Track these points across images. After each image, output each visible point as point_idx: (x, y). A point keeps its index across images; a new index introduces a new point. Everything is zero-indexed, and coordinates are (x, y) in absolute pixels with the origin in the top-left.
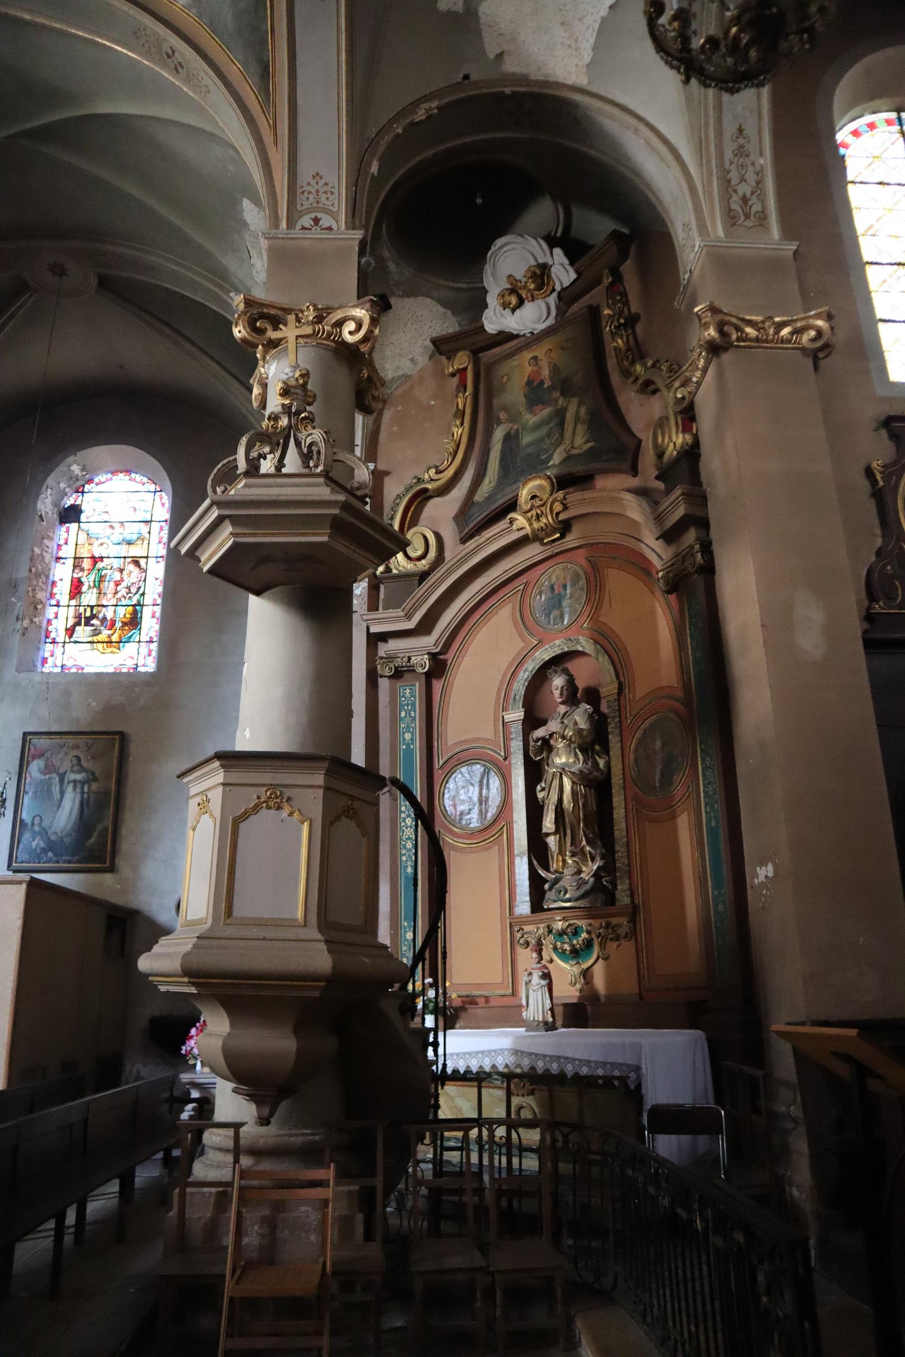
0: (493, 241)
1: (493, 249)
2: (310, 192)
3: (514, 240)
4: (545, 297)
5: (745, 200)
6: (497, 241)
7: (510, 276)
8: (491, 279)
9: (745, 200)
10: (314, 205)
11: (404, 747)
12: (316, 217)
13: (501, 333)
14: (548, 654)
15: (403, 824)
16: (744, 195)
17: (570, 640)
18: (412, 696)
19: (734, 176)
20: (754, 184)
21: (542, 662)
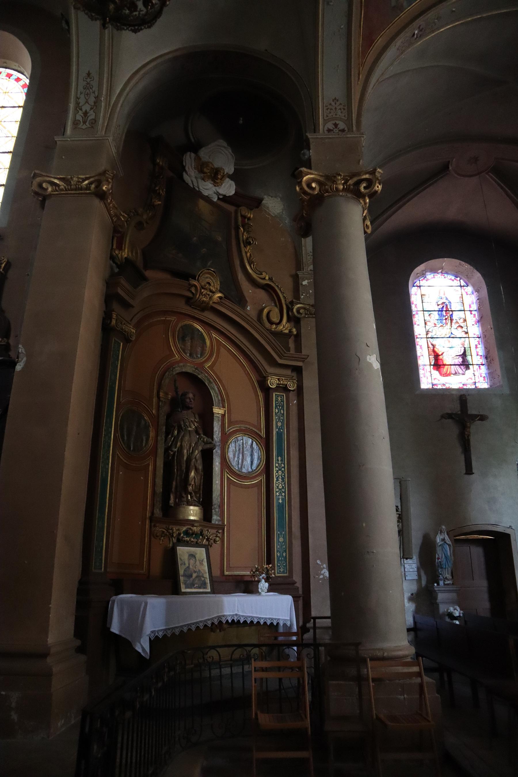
2: (331, 109)
5: (86, 113)
9: (86, 113)
10: (334, 116)
11: (283, 533)
12: (336, 123)
15: (283, 485)
16: (86, 111)
18: (279, 566)
19: (82, 101)
20: (93, 104)
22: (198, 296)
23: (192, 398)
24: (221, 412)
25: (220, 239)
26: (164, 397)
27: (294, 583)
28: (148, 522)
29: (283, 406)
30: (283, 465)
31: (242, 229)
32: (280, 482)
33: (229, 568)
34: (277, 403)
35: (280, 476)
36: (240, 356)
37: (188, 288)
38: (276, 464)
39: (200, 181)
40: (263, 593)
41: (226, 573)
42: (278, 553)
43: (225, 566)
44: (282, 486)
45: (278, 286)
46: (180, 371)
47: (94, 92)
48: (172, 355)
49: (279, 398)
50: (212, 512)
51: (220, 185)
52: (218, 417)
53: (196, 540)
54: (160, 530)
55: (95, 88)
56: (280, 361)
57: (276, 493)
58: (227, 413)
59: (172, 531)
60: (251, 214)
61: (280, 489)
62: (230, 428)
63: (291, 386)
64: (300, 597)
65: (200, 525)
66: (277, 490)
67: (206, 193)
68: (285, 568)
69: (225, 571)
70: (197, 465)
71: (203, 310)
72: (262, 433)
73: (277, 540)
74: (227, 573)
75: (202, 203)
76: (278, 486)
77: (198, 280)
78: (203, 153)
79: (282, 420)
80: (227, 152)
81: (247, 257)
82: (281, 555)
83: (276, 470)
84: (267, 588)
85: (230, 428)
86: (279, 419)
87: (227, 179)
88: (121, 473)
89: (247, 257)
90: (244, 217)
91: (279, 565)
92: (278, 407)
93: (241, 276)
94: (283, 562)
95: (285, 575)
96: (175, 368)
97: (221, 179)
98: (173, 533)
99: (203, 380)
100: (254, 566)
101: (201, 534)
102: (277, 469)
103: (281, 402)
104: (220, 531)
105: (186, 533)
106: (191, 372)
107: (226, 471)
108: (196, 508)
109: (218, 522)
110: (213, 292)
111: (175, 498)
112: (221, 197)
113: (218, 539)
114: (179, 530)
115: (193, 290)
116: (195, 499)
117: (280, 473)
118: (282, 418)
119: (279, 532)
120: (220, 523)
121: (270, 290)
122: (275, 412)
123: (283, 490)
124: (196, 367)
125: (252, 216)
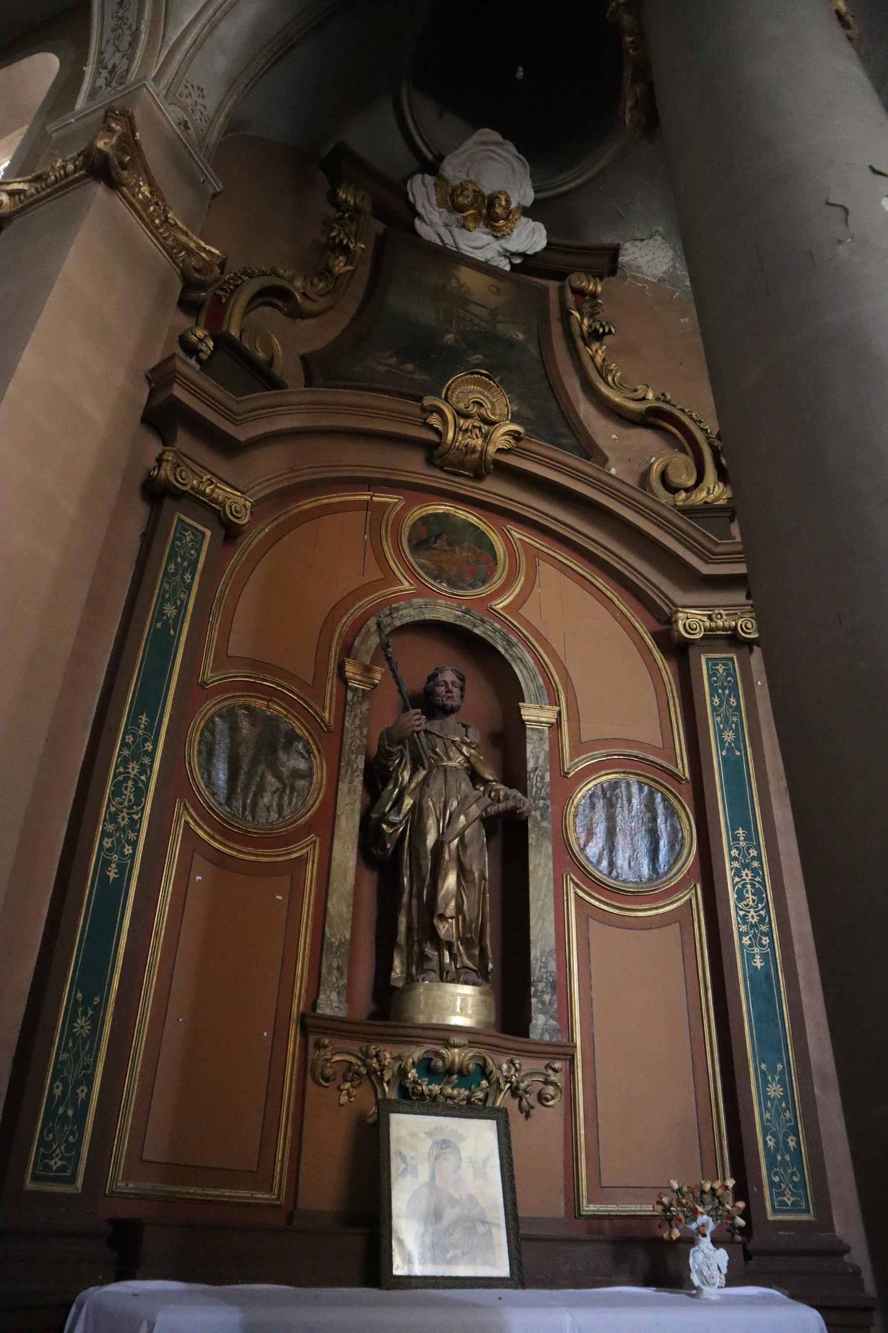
11: (779, 1066)
15: (762, 913)
22: (450, 435)
23: (453, 683)
24: (548, 715)
25: (521, 337)
26: (358, 677)
27: (840, 1250)
28: (293, 1030)
29: (734, 688)
30: (753, 853)
31: (577, 315)
32: (751, 903)
33: (598, 1191)
34: (716, 682)
35: (749, 886)
36: (595, 579)
37: (422, 421)
38: (730, 850)
39: (457, 231)
40: (711, 1292)
41: (589, 1208)
42: (768, 1138)
43: (584, 1184)
44: (760, 915)
45: (682, 410)
46: (417, 619)
47: (130, 27)
48: (390, 579)
49: (721, 668)
50: (530, 1004)
51: (509, 234)
52: (541, 732)
53: (467, 1093)
54: (337, 1058)
55: (132, 20)
56: (706, 569)
57: (741, 940)
58: (568, 720)
59: (379, 1061)
60: (595, 285)
61: (752, 926)
62: (577, 760)
63: (748, 629)
64: (868, 1310)
65: (469, 1042)
66: (744, 928)
67: (480, 255)
68: (801, 1191)
69: (584, 1202)
70: (466, 861)
71: (478, 477)
72: (680, 766)
73: (759, 1094)
74: (592, 1207)
75: (466, 274)
76: (745, 915)
77: (446, 399)
78: (452, 169)
79: (182, 602)
80: (504, 154)
81: (596, 366)
82: (781, 1146)
83: (732, 869)
84: (725, 1271)
85: (577, 760)
86: (726, 721)
87: (524, 220)
88: (199, 878)
89: (596, 366)
90: (579, 293)
91: (776, 1179)
92: (720, 691)
93: (585, 410)
94: (789, 1171)
95: (805, 1217)
96: (397, 609)
97: (506, 219)
98: (383, 1068)
99: (490, 640)
100: (666, 1185)
101: (483, 1072)
102: (736, 864)
103: (726, 677)
104: (557, 1065)
105: (427, 1067)
106: (451, 620)
107: (571, 879)
108: (467, 990)
109: (551, 1037)
110: (491, 423)
111: (408, 965)
112: (517, 261)
113: (550, 1090)
114: (399, 1058)
115: (434, 420)
116: (468, 963)
117: (747, 875)
118: (735, 719)
119: (763, 1066)
120: (557, 1039)
121: (665, 424)
122: (712, 704)
123: (764, 928)
124: (464, 607)
125: (599, 289)
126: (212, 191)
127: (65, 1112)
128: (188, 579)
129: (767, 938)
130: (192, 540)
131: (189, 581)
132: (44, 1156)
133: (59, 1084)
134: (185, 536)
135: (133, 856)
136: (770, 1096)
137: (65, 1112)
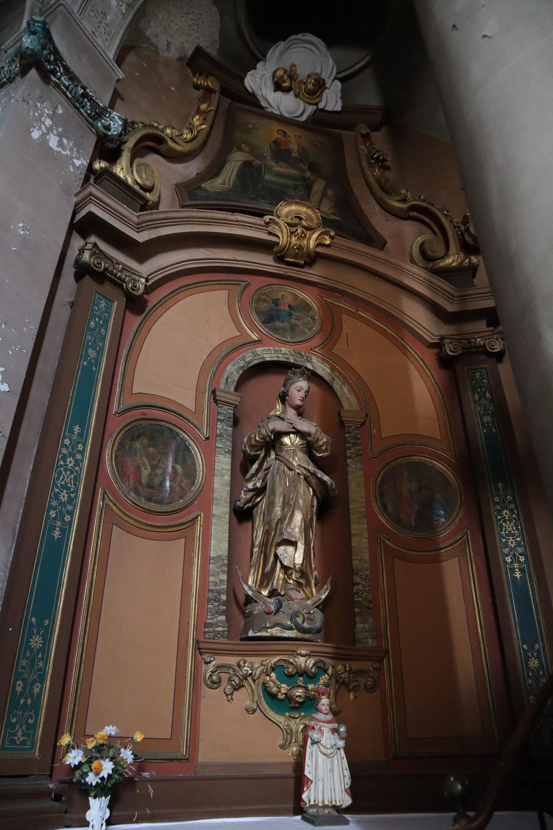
0: (309, 32)
1: (300, 36)
3: (319, 46)
4: (307, 103)
6: (309, 35)
7: (293, 65)
8: (277, 54)
13: (253, 95)
14: (269, 355)
15: (62, 463)
17: (301, 354)
21: (261, 360)
44: (65, 462)
76: (512, 515)
79: (100, 348)
103: (104, 312)
126: (116, 78)
127: (25, 702)
128: (103, 332)
129: (523, 557)
130: (105, 307)
131: (104, 334)
132: (11, 734)
133: (20, 682)
134: (101, 304)
135: (71, 523)
136: (531, 667)
137: (25, 702)
